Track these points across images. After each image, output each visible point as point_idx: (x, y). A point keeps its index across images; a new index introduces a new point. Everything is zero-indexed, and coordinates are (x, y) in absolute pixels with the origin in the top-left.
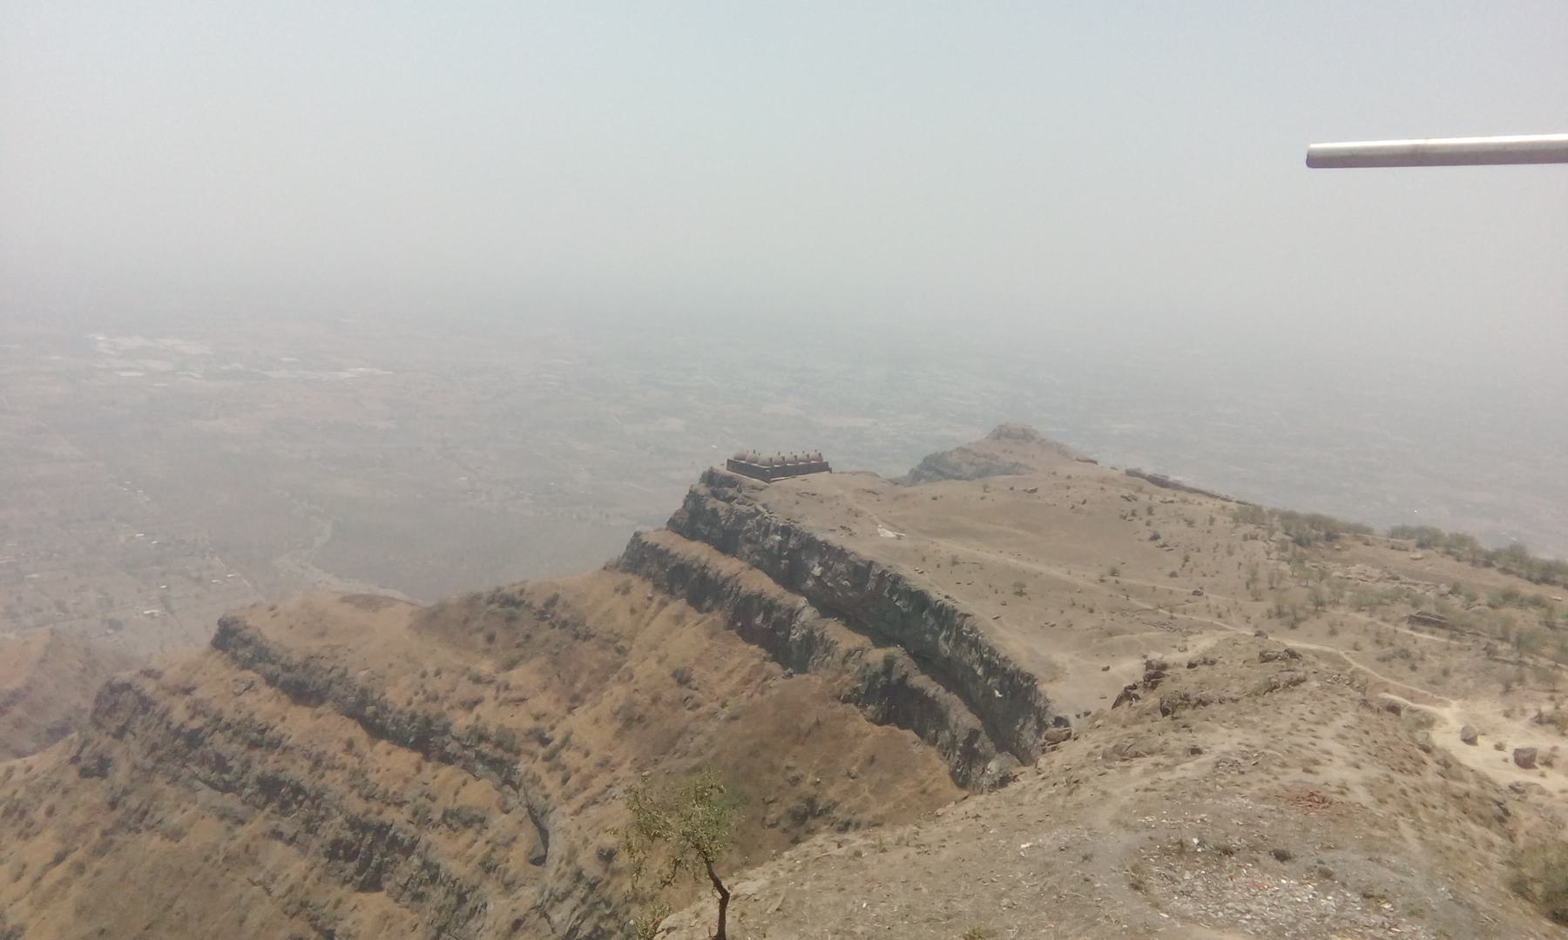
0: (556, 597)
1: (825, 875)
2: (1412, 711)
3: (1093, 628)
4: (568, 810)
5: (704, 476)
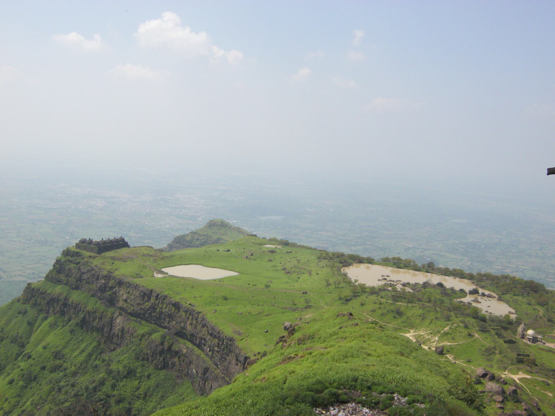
5: (64, 252)
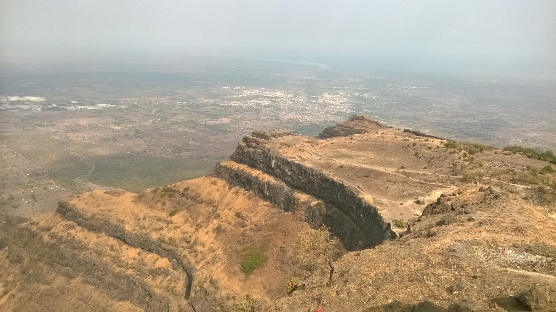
0: (188, 187)
1: (241, 211)
2: (388, 195)
3: (396, 189)
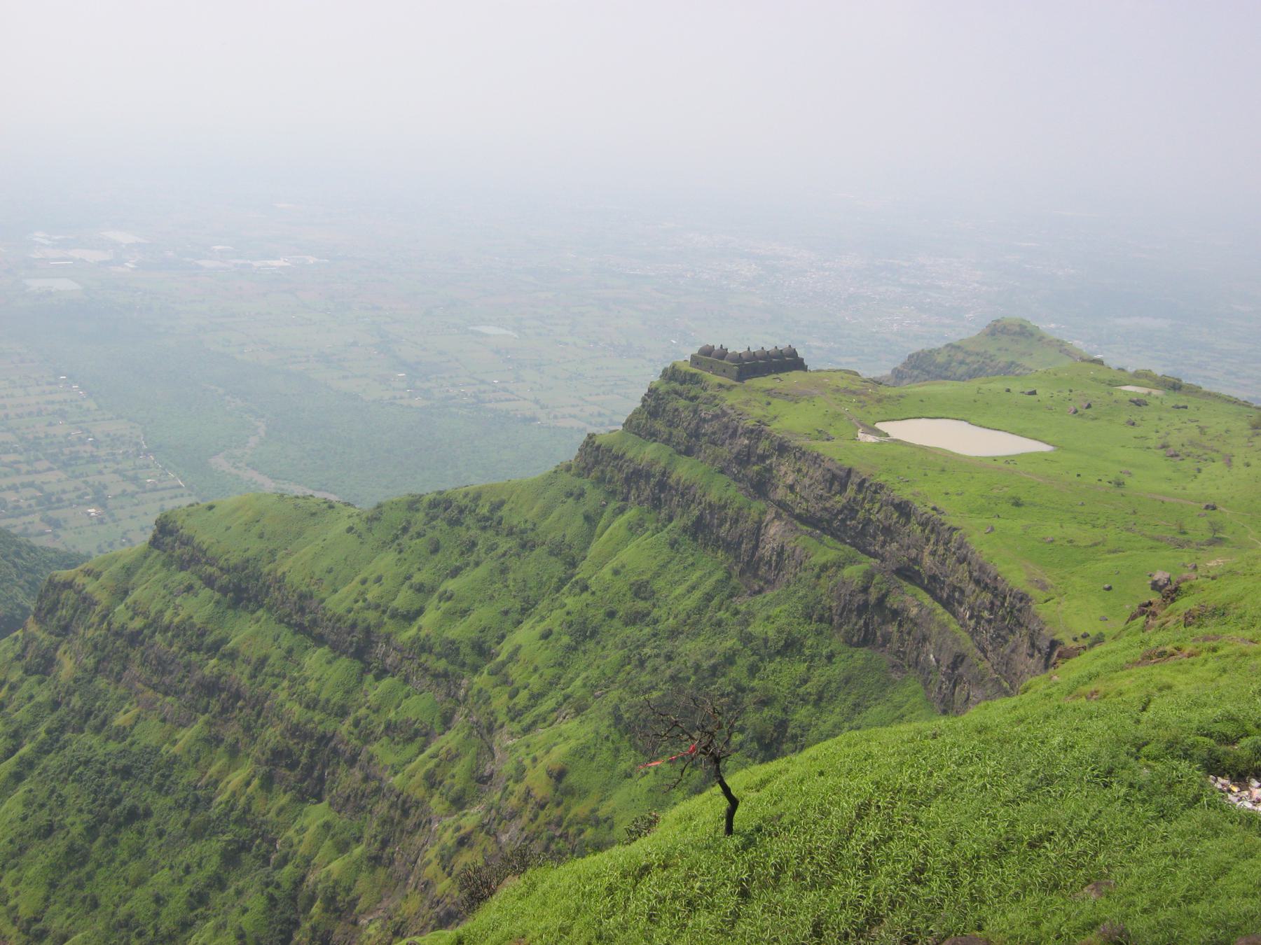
4: (516, 727)
5: (665, 371)
